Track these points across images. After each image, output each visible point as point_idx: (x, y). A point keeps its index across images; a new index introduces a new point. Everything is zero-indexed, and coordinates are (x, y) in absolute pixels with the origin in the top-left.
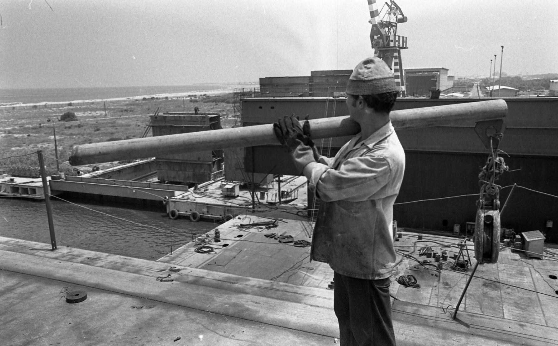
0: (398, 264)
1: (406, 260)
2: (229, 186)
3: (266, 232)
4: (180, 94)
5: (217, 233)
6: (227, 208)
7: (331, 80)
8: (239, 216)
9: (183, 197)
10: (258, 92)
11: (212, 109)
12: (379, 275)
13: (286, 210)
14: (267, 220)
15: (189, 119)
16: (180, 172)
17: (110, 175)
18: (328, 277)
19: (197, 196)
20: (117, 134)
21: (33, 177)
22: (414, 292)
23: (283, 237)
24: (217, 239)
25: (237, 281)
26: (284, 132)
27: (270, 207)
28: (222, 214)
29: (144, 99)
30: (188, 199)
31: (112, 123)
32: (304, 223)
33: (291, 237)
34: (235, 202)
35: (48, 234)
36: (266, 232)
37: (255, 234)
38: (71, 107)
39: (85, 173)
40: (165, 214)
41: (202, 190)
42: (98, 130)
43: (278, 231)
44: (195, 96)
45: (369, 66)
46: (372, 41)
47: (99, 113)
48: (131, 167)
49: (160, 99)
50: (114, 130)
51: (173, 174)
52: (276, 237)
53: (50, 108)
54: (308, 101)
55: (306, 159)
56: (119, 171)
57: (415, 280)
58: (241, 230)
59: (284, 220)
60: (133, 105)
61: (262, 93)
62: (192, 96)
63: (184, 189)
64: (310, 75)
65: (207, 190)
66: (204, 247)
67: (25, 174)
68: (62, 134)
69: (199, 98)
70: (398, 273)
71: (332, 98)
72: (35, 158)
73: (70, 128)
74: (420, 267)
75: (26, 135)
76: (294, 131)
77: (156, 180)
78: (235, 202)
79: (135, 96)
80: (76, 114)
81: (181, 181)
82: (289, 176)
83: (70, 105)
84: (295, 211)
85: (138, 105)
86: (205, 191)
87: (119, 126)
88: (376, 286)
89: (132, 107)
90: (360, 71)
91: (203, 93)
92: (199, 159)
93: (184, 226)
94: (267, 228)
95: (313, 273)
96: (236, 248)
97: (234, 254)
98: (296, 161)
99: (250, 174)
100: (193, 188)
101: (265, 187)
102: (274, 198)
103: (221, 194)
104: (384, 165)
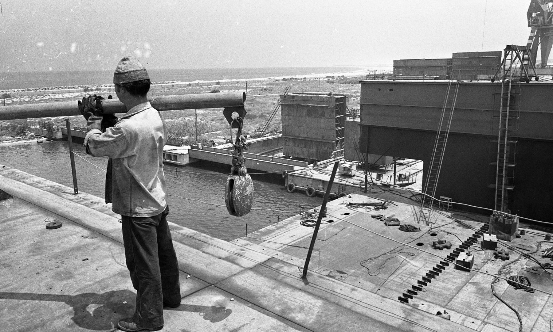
0: (512, 262)
1: (524, 260)
2: (347, 164)
3: (374, 212)
4: (318, 75)
7: (474, 62)
9: (302, 172)
10: (391, 75)
11: (347, 90)
12: (136, 213)
13: (400, 193)
14: (377, 201)
15: (316, 99)
16: (304, 149)
18: (427, 265)
19: (314, 172)
21: (177, 146)
22: (524, 296)
23: (390, 220)
27: (383, 188)
30: (306, 174)
32: (416, 207)
33: (397, 220)
34: (350, 181)
35: (72, 180)
36: (374, 212)
39: (219, 144)
40: (284, 187)
43: (386, 213)
44: (333, 77)
45: (125, 62)
46: (529, 19)
48: (260, 141)
49: (298, 79)
51: (297, 150)
52: (383, 219)
53: (201, 86)
57: (529, 283)
58: (349, 209)
59: (395, 203)
60: (273, 84)
61: (395, 76)
62: (330, 77)
63: (304, 165)
64: (451, 57)
65: (326, 167)
66: (310, 221)
69: (337, 79)
70: (509, 273)
71: (455, 81)
72: (65, 123)
74: (539, 269)
77: (281, 154)
78: (350, 181)
79: (275, 76)
82: (411, 160)
83: (218, 83)
84: (409, 195)
85: (277, 84)
88: (134, 222)
90: (120, 66)
91: (341, 75)
92: (323, 137)
93: (298, 200)
94: (375, 209)
95: (413, 259)
97: (336, 230)
99: (365, 154)
100: (312, 165)
101: (384, 168)
104: (119, 133)
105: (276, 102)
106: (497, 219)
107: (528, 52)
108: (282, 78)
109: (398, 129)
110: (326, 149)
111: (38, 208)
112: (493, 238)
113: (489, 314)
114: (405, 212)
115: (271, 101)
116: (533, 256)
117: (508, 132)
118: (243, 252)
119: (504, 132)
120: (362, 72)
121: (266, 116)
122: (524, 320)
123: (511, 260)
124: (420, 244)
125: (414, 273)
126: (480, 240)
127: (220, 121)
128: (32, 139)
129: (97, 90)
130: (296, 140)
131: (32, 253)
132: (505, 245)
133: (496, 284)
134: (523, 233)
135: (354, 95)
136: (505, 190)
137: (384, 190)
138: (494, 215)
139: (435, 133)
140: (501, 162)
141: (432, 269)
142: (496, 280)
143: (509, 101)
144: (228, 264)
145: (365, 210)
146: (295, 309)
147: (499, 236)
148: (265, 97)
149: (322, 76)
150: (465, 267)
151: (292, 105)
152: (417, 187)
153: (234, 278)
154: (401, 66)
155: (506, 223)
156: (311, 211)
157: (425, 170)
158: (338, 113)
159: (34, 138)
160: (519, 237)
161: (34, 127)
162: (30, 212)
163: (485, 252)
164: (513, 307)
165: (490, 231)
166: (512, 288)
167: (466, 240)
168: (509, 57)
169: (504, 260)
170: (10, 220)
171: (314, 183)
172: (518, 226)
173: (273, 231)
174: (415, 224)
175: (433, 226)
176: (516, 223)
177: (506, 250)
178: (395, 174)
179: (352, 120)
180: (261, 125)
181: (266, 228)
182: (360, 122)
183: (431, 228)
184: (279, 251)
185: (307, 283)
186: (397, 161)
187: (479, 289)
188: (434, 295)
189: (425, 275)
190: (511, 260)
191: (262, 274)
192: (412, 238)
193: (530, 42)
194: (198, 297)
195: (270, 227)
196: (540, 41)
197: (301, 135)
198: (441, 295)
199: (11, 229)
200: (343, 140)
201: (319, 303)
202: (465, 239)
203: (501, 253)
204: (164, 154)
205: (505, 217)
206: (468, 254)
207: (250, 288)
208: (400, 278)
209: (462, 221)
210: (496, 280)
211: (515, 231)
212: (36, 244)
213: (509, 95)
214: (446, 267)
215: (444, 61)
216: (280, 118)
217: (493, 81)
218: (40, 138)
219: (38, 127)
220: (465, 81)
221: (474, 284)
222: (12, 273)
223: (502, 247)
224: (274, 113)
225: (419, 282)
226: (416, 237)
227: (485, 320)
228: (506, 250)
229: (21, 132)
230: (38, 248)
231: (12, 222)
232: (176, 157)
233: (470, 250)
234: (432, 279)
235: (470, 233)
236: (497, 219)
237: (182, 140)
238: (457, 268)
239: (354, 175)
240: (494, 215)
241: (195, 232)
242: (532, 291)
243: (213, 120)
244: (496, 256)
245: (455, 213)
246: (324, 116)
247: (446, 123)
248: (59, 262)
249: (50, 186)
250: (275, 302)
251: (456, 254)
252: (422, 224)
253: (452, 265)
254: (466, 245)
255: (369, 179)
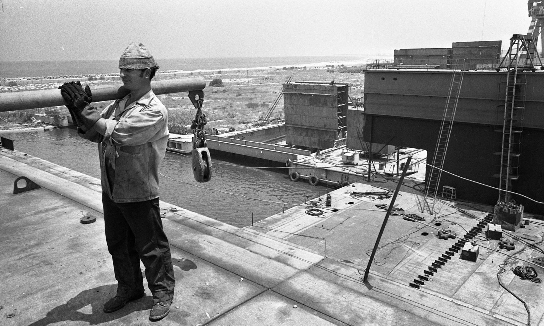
0: (517, 253)
1: (529, 250)
2: (349, 153)
3: (378, 202)
4: (317, 65)
5: (329, 198)
6: (344, 175)
7: (475, 52)
8: (354, 184)
9: (305, 161)
10: (391, 64)
11: (347, 79)
14: (380, 190)
16: (306, 138)
17: (244, 136)
18: (432, 255)
20: (255, 99)
21: (181, 134)
24: (328, 204)
25: (212, 225)
26: (73, 97)
28: (340, 181)
29: (285, 68)
30: (309, 163)
31: (252, 89)
32: (419, 196)
33: (402, 209)
34: (353, 170)
36: (378, 202)
37: (366, 203)
38: (220, 75)
40: (286, 176)
41: (324, 156)
42: (239, 95)
44: (333, 66)
46: (529, 9)
47: (242, 80)
48: (263, 130)
49: (299, 68)
50: (253, 96)
51: (300, 139)
53: (203, 75)
54: (404, 72)
55: (96, 116)
56: (252, 133)
57: (536, 273)
58: (353, 198)
60: (272, 73)
61: (395, 65)
62: (330, 66)
64: (451, 47)
65: (328, 156)
66: (315, 210)
67: (175, 131)
68: (209, 98)
69: (336, 68)
70: (515, 263)
71: (460, 71)
73: (216, 92)
75: (181, 98)
76: (80, 95)
77: (284, 143)
80: (223, 81)
81: (306, 146)
82: (413, 149)
83: (220, 72)
84: (412, 185)
85: (278, 73)
86: (326, 157)
87: (258, 92)
89: (273, 75)
92: (325, 126)
93: (301, 188)
94: (379, 198)
95: (419, 248)
96: (345, 214)
97: (342, 219)
98: (87, 119)
100: (315, 154)
101: (386, 157)
102: (392, 170)
103: (341, 161)
105: (278, 91)
106: (502, 209)
107: (529, 41)
108: (282, 67)
109: (402, 118)
110: (327, 138)
111: (68, 200)
112: (498, 228)
113: (496, 305)
114: (408, 201)
115: (272, 90)
116: (538, 246)
117: (513, 121)
118: (293, 251)
119: (508, 121)
120: (363, 60)
121: (269, 105)
122: (531, 310)
123: (516, 250)
124: (425, 234)
125: (420, 263)
126: (485, 230)
127: (223, 110)
128: (39, 126)
129: (101, 79)
130: (298, 129)
131: (71, 251)
132: (510, 235)
133: (502, 274)
134: (527, 223)
135: (354, 84)
136: (509, 179)
137: (387, 179)
138: (498, 205)
139: (439, 122)
140: (506, 152)
141: (437, 259)
142: (502, 270)
143: (514, 90)
144: (280, 265)
145: (368, 199)
146: (366, 318)
147: (504, 226)
148: (266, 86)
149: (322, 65)
150: (470, 257)
151: (294, 93)
152: (420, 176)
153: (290, 281)
154: (402, 55)
155: (511, 213)
156: (316, 200)
157: (429, 159)
158: (339, 102)
159: (41, 125)
160: (524, 227)
161: (40, 115)
162: (61, 204)
163: (490, 243)
164: (520, 297)
165: (494, 221)
166: (518, 278)
167: (470, 230)
168: (515, 46)
169: (509, 250)
170: (41, 212)
171: (318, 172)
172: (522, 215)
173: (279, 220)
174: (419, 213)
175: (437, 216)
176: (521, 213)
177: (511, 240)
178: (398, 163)
179: (354, 109)
180: (263, 113)
181: (272, 216)
182: (364, 111)
183: (435, 218)
184: (285, 240)
185: (370, 288)
186: (400, 150)
187: (484, 280)
188: (440, 284)
189: (431, 265)
190: (516, 250)
191: (319, 277)
192: (417, 228)
193: (531, 31)
194: (257, 303)
195: (275, 216)
196: (540, 31)
197: (305, 124)
198: (448, 285)
199: (42, 222)
200: (345, 129)
201: (390, 311)
202: (469, 229)
203: (506, 243)
204: (168, 142)
205: (509, 207)
206: (474, 245)
207: (312, 293)
208: (407, 268)
209: (466, 210)
210: (502, 270)
211: (519, 221)
212: (72, 240)
213: (515, 84)
214: (451, 257)
215: (445, 50)
216: (283, 106)
217: (498, 70)
218: (47, 125)
219: (45, 115)
220: (470, 71)
221: (480, 274)
222: (54, 272)
223: (507, 237)
224: (276, 103)
225: (425, 272)
226: (420, 226)
227: (493, 311)
228: (511, 240)
229: (28, 120)
230: (76, 244)
231: (44, 214)
232: (180, 145)
233: (475, 240)
234: (438, 269)
235: (474, 223)
236: (502, 209)
237: (186, 128)
238: (463, 257)
239: (357, 164)
240: (498, 205)
241: (236, 228)
242: (539, 281)
243: (215, 109)
244: (502, 246)
245: (459, 202)
246: (326, 105)
247: (450, 114)
248: (101, 261)
249: (76, 177)
250: (342, 310)
251: (462, 243)
252: (426, 214)
253: (457, 255)
254: (470, 235)
255: (372, 169)
